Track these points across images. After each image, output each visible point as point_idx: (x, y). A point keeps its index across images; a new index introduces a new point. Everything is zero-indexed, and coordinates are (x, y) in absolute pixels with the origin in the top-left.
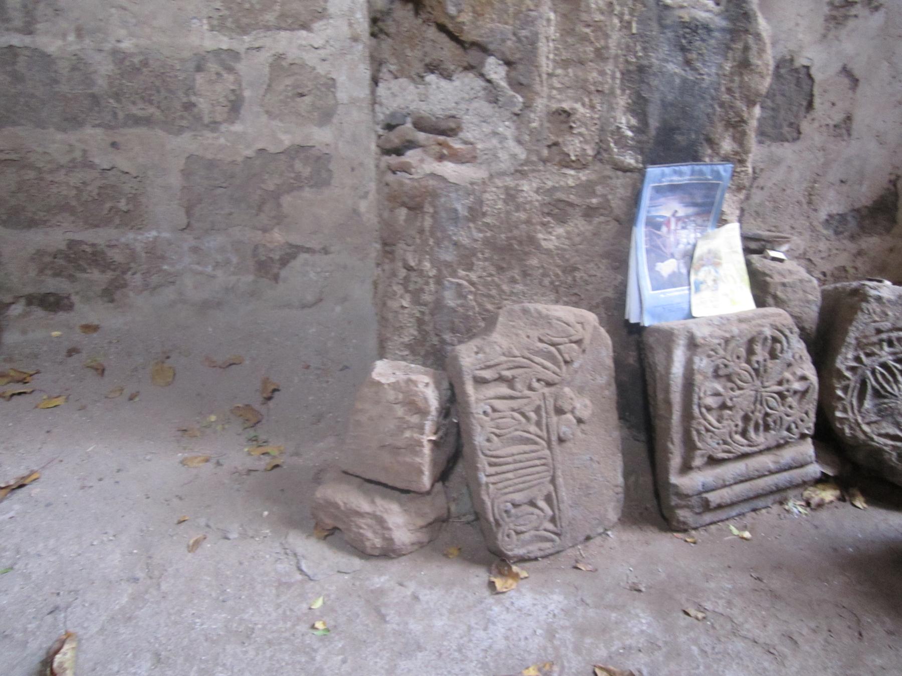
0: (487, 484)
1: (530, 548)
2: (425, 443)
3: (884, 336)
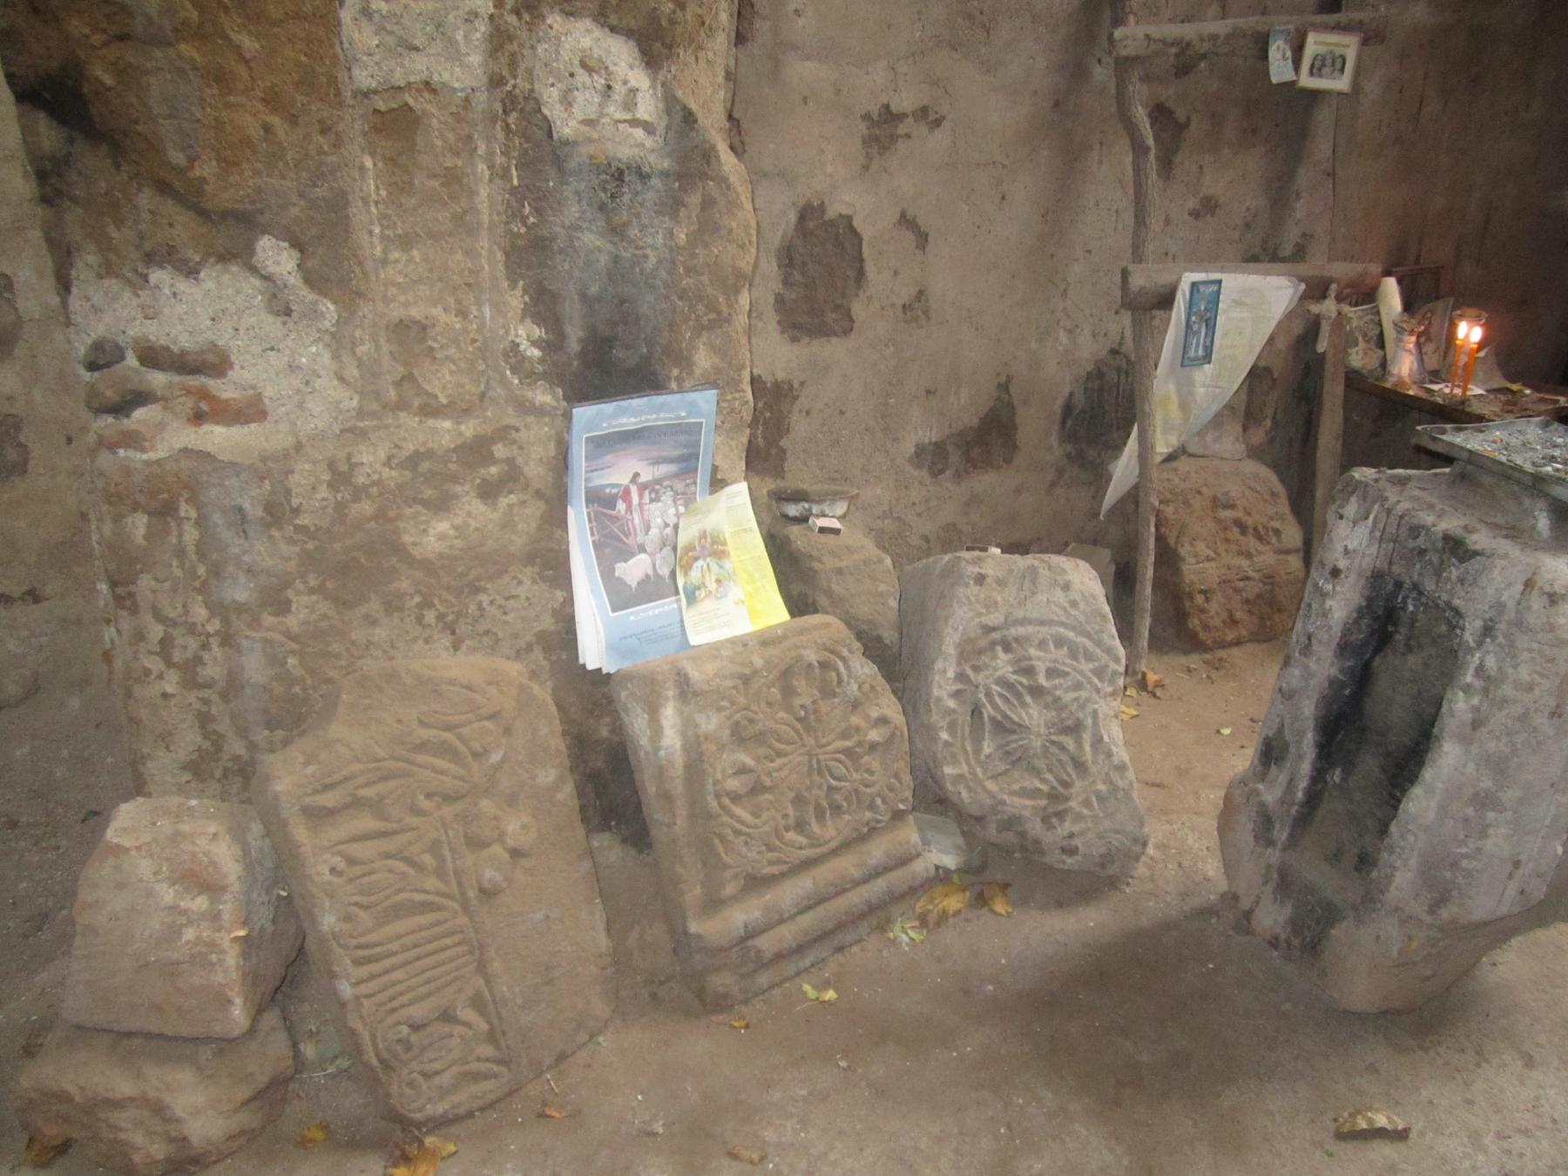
0: (357, 998)
1: (455, 1099)
2: (226, 944)
3: (996, 636)
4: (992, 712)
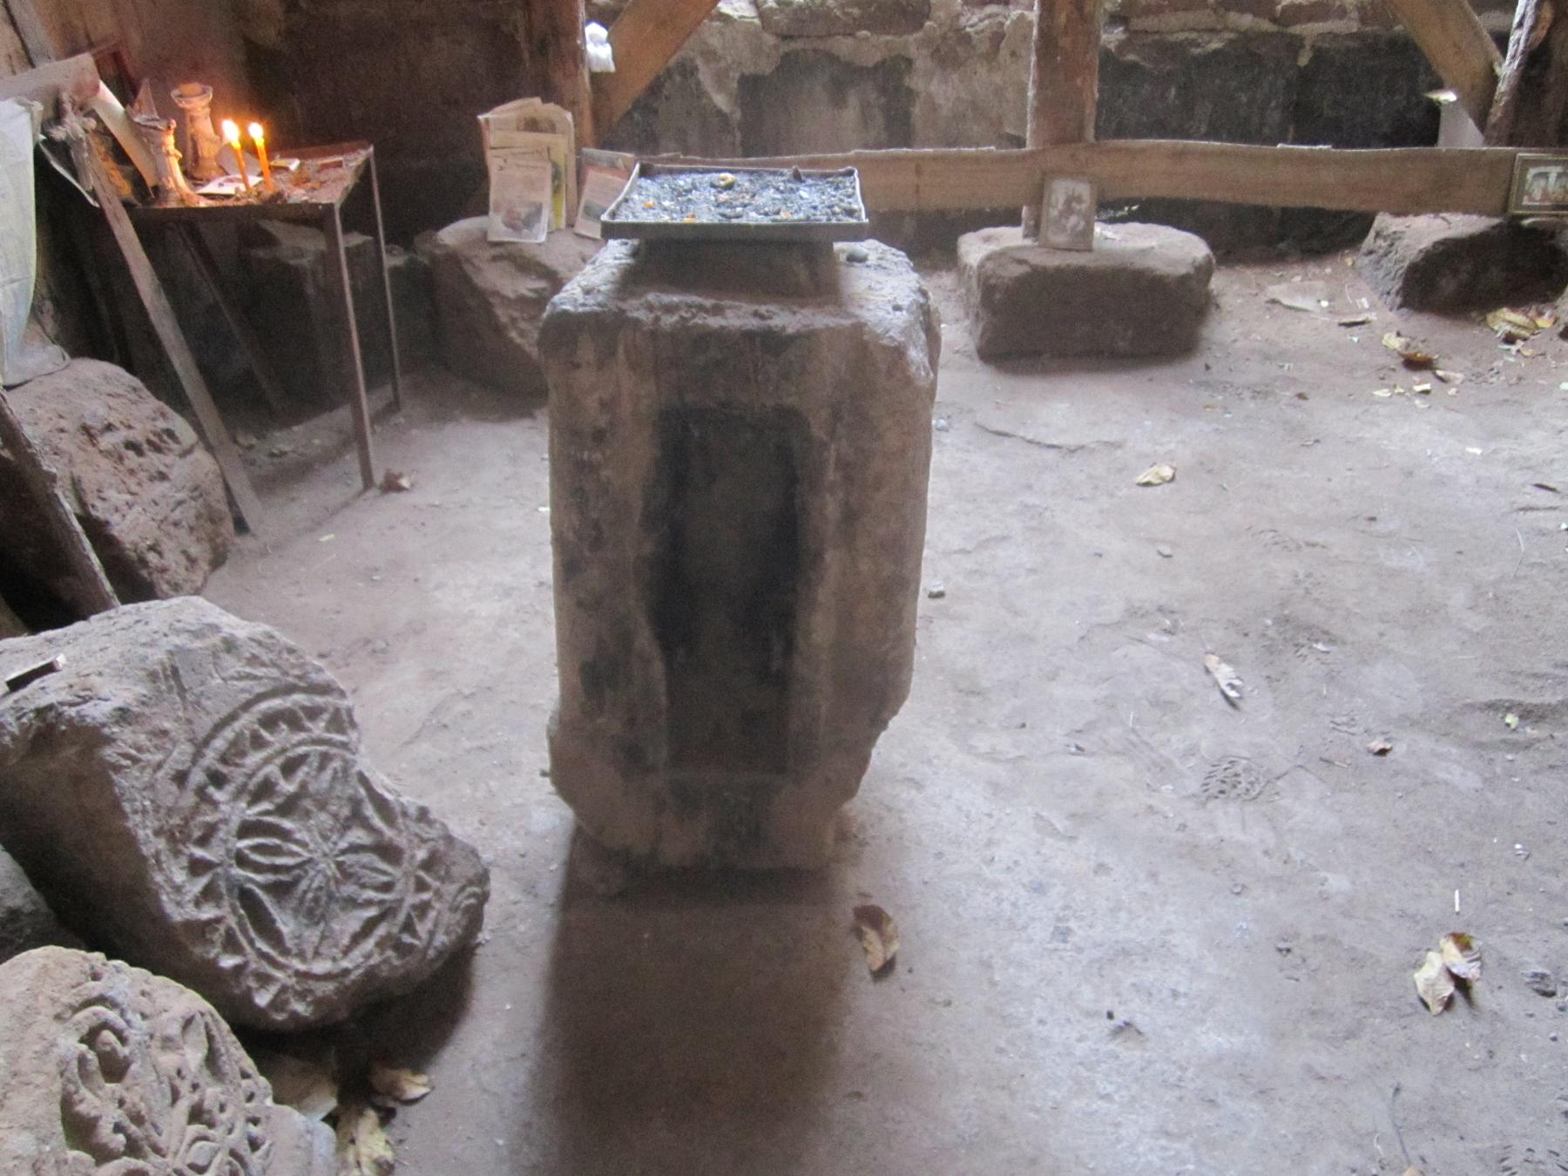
4: (259, 878)
